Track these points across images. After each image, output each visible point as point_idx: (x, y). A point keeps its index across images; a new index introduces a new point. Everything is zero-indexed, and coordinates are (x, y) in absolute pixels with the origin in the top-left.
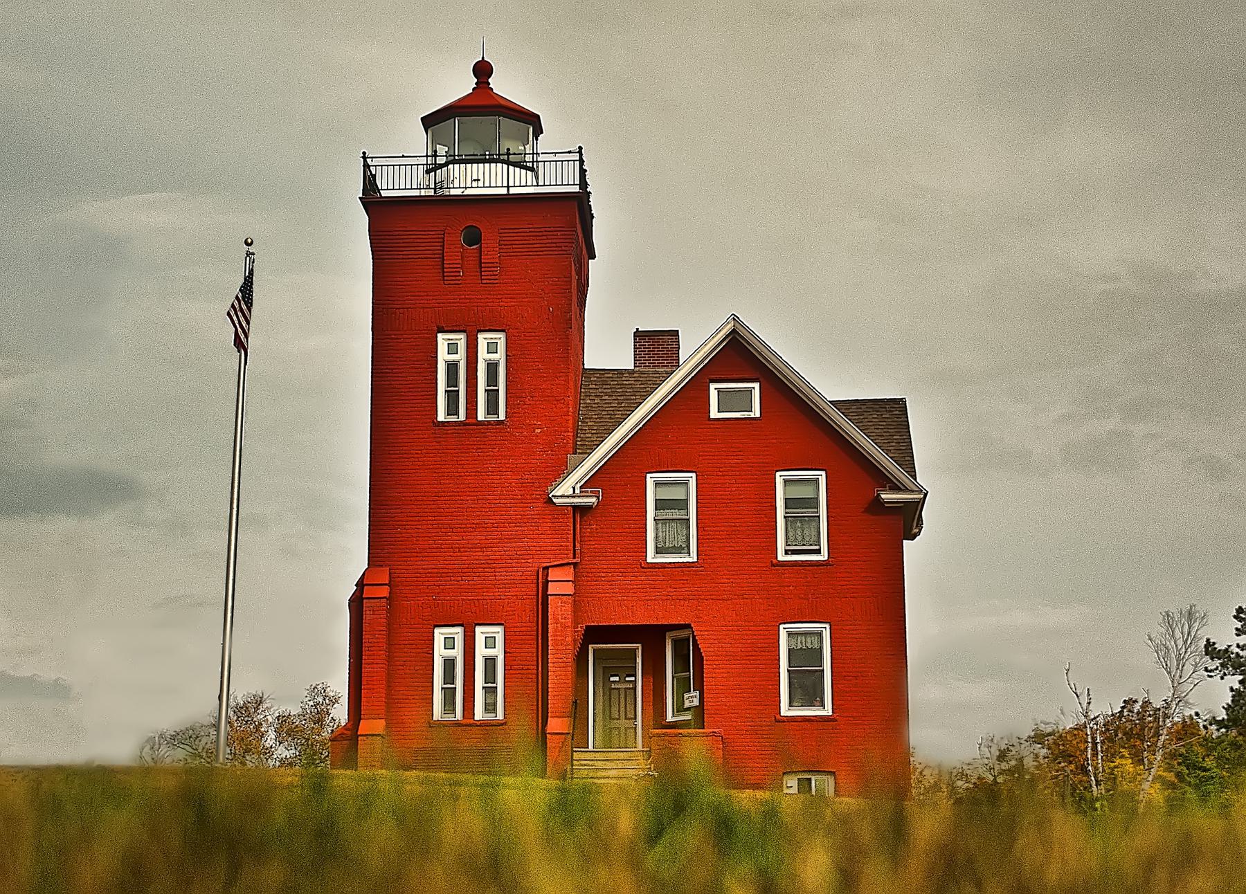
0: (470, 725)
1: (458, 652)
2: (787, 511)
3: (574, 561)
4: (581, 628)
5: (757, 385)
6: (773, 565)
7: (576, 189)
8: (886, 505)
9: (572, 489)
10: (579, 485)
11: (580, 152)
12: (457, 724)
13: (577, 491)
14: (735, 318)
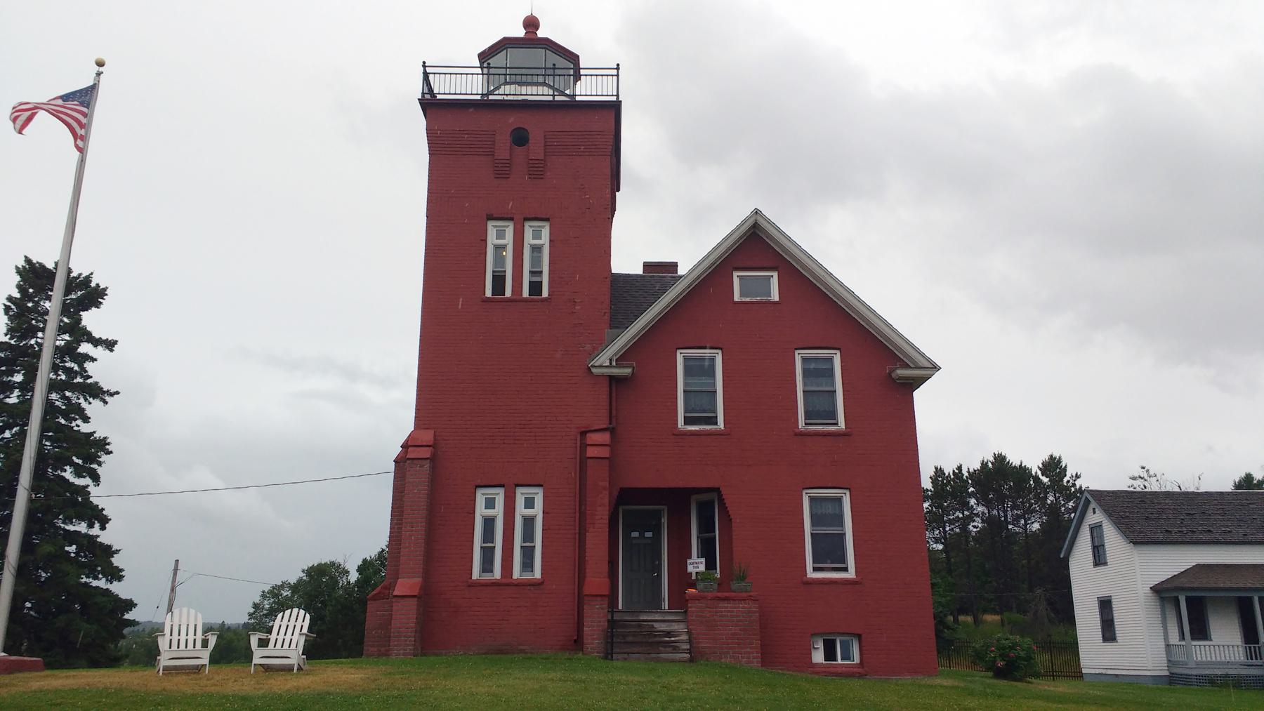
0: (508, 585)
1: (498, 511)
2: (808, 421)
3: (611, 426)
5: (775, 274)
6: (796, 435)
7: (614, 99)
11: (618, 68)
12: (495, 584)
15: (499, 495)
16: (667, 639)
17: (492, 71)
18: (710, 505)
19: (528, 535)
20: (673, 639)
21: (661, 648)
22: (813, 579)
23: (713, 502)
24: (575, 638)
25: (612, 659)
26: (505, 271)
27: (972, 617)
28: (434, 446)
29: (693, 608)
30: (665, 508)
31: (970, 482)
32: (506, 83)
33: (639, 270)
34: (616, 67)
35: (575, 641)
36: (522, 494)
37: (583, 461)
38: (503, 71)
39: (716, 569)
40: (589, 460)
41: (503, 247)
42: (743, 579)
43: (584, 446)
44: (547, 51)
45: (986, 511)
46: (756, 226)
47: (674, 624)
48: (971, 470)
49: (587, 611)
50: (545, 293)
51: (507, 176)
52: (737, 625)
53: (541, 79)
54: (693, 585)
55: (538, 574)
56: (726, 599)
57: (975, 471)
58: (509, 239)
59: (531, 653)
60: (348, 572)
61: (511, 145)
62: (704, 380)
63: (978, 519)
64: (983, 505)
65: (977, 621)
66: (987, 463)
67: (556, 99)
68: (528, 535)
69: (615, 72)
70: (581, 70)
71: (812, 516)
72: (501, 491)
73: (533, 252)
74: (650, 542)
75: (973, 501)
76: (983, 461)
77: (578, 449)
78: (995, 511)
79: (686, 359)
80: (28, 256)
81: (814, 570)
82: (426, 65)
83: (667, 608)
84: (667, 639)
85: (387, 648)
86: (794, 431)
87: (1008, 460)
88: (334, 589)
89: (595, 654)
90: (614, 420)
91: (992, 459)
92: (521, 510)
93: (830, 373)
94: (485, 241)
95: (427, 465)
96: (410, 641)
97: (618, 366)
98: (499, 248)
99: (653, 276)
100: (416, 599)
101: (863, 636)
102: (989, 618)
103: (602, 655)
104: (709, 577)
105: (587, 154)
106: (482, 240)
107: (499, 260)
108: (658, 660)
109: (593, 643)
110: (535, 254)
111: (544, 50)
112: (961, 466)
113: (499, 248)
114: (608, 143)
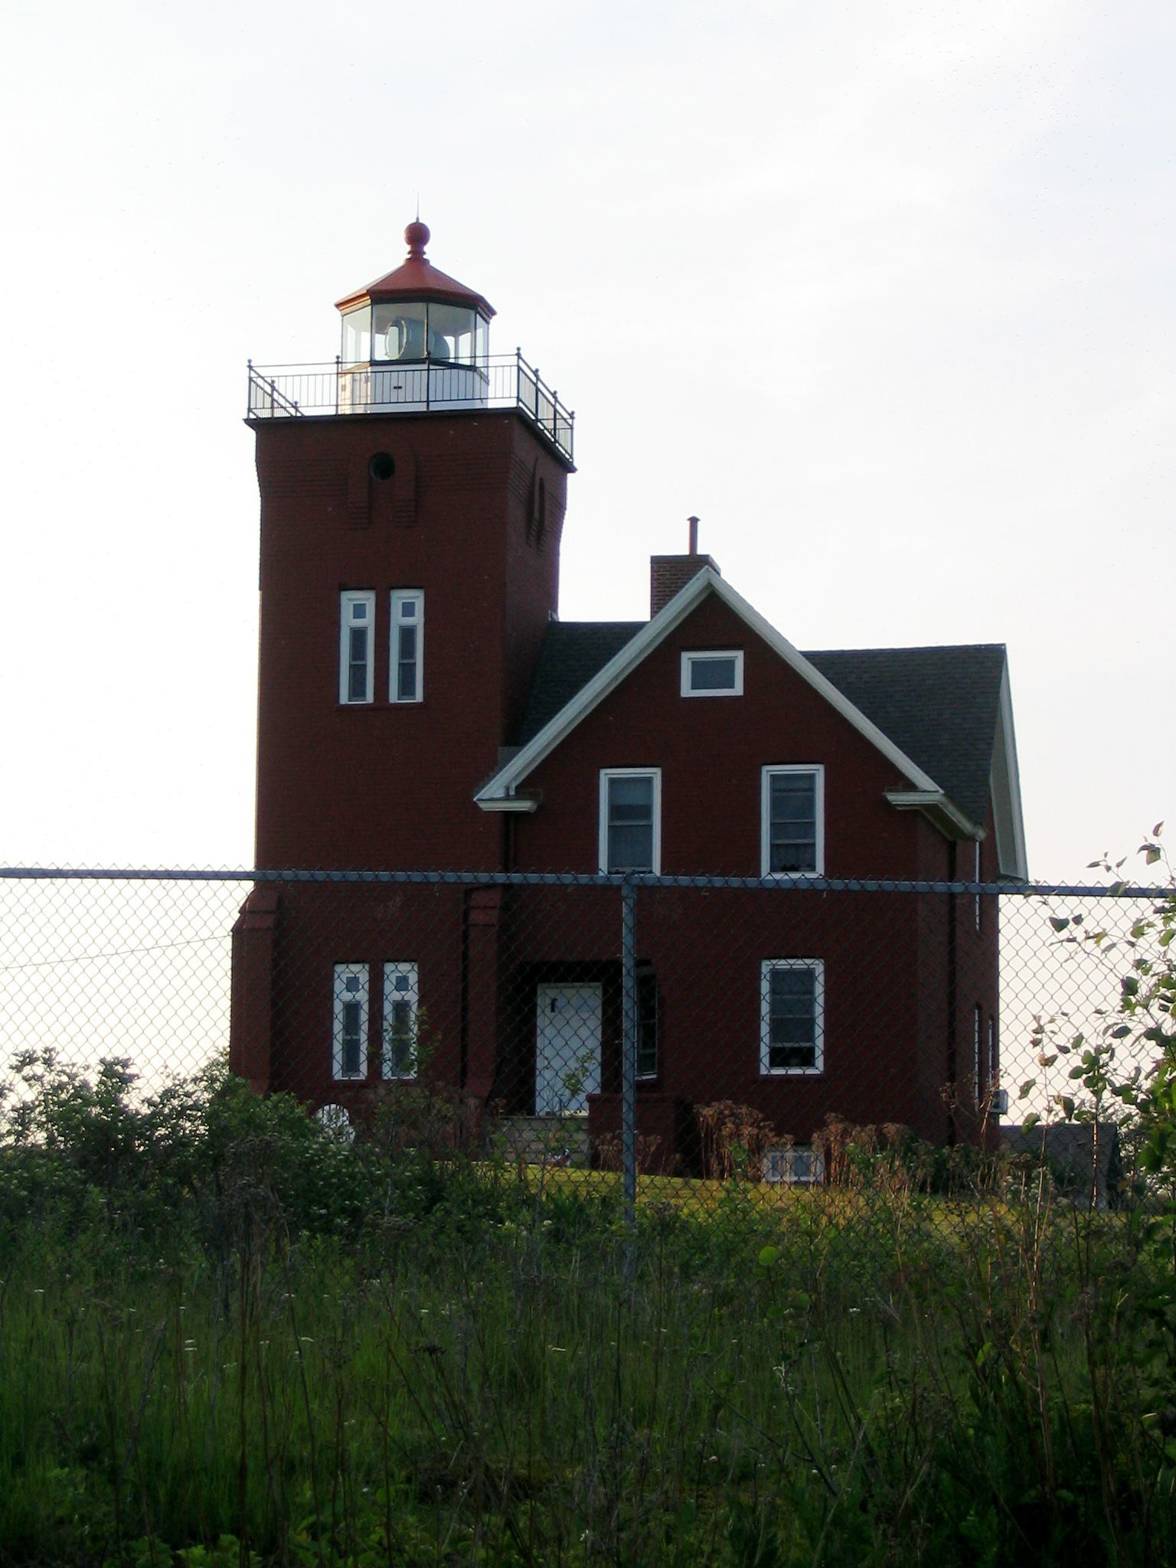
1: (369, 622)
10: (514, 786)
19: (407, 649)
55: (419, 697)
68: (407, 649)
80: (550, 380)
92: (397, 620)
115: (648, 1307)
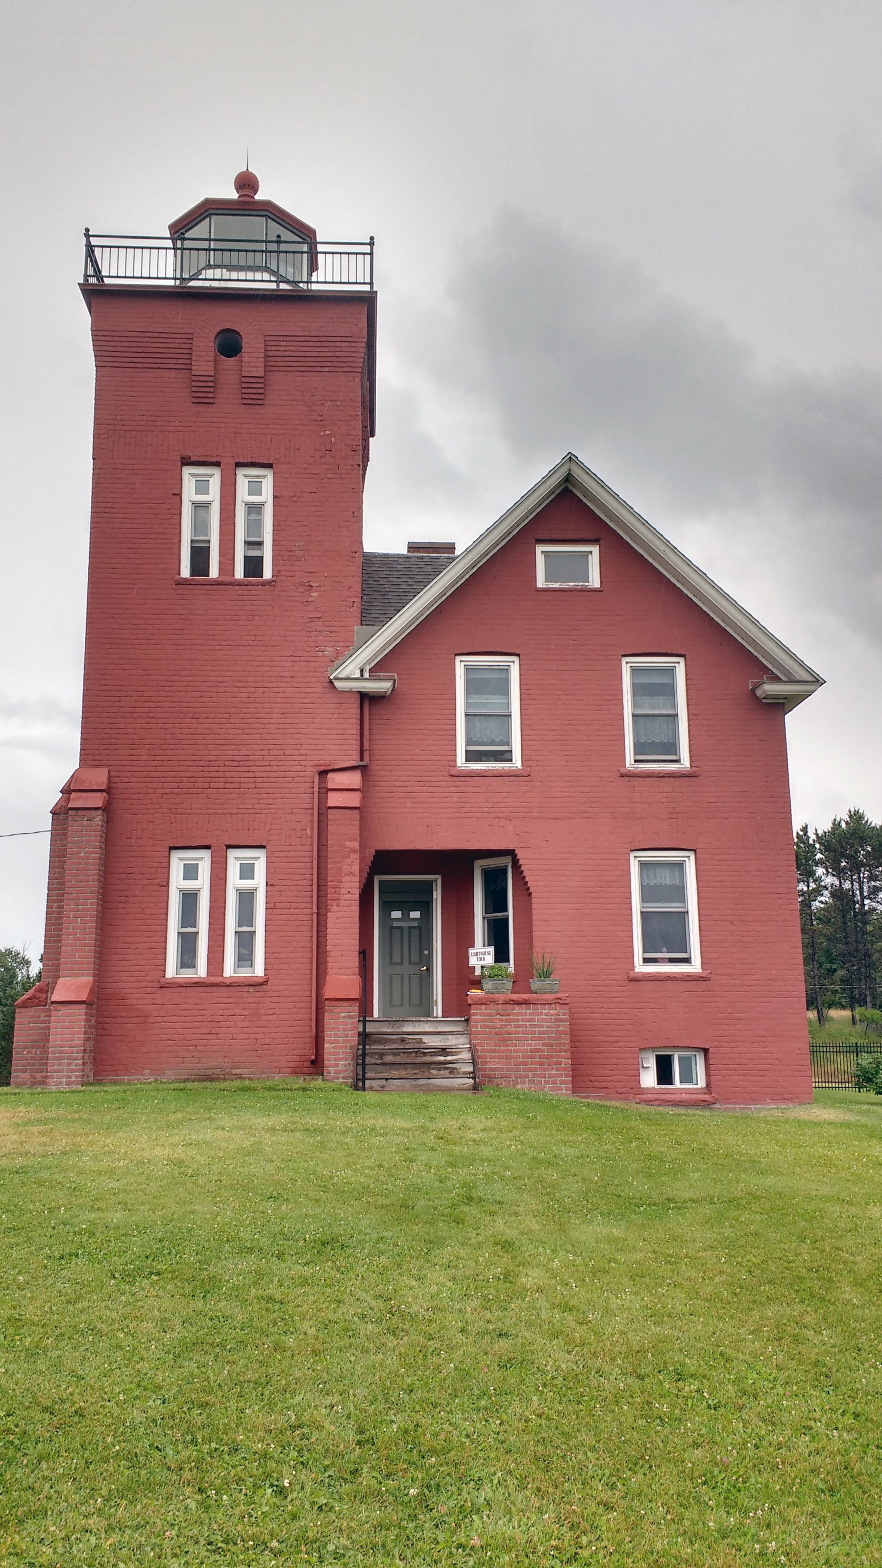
1: (203, 882)
3: (363, 763)
4: (370, 854)
5: (595, 549)
7: (367, 288)
8: (764, 701)
9: (359, 671)
10: (368, 668)
11: (371, 243)
12: (198, 984)
13: (367, 675)
14: (571, 458)
15: (204, 860)
16: (442, 1058)
17: (187, 244)
18: (502, 872)
19: (246, 915)
20: (449, 1058)
21: (432, 1071)
22: (644, 974)
23: (504, 871)
24: (313, 1057)
25: (363, 1088)
26: (209, 541)
27: (815, 1012)
28: (108, 791)
29: (478, 1015)
30: (439, 878)
31: (817, 846)
32: (209, 266)
33: (404, 551)
34: (368, 241)
35: (313, 1062)
36: (236, 858)
37: (323, 812)
38: (205, 244)
39: (508, 960)
40: (330, 811)
41: (206, 505)
42: (547, 975)
43: (324, 791)
44: (269, 220)
45: (837, 883)
46: (569, 478)
47: (450, 1037)
48: (820, 832)
49: (328, 1018)
50: (268, 574)
51: (211, 401)
52: (539, 1039)
53: (260, 259)
54: (477, 983)
55: (259, 970)
56: (526, 1003)
57: (825, 833)
58: (214, 494)
59: (250, 1079)
60: (27, 963)
61: (216, 355)
62: (496, 700)
63: (826, 893)
64: (834, 875)
65: (821, 1018)
66: (840, 822)
67: (281, 288)
68: (246, 915)
69: (367, 249)
70: (318, 245)
71: (643, 888)
72: (206, 855)
73: (249, 514)
74: (416, 924)
75: (820, 871)
76: (835, 820)
77: (316, 795)
78: (848, 882)
79: (468, 670)
81: (644, 962)
82: (90, 233)
83: (440, 1014)
84: (442, 1058)
85: (44, 1074)
86: (619, 771)
87: (866, 819)
88: (11, 983)
89: (341, 1080)
90: (366, 754)
91: (846, 817)
92: (234, 881)
93: (670, 690)
94: (179, 495)
95: (98, 818)
96: (77, 1065)
97: (372, 678)
98: (201, 507)
99: (422, 557)
100: (84, 1006)
101: (711, 1050)
102: (835, 1013)
103: (350, 1080)
104: (500, 972)
105: (327, 369)
106: (175, 494)
107: (200, 525)
108: (430, 1090)
109: (337, 1065)
110: (253, 517)
111: (264, 218)
112: (806, 826)
113: (201, 507)
114: (357, 354)
115: (791, 1500)
